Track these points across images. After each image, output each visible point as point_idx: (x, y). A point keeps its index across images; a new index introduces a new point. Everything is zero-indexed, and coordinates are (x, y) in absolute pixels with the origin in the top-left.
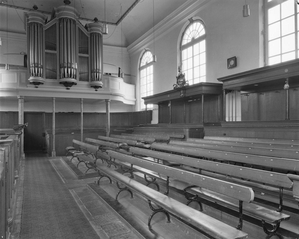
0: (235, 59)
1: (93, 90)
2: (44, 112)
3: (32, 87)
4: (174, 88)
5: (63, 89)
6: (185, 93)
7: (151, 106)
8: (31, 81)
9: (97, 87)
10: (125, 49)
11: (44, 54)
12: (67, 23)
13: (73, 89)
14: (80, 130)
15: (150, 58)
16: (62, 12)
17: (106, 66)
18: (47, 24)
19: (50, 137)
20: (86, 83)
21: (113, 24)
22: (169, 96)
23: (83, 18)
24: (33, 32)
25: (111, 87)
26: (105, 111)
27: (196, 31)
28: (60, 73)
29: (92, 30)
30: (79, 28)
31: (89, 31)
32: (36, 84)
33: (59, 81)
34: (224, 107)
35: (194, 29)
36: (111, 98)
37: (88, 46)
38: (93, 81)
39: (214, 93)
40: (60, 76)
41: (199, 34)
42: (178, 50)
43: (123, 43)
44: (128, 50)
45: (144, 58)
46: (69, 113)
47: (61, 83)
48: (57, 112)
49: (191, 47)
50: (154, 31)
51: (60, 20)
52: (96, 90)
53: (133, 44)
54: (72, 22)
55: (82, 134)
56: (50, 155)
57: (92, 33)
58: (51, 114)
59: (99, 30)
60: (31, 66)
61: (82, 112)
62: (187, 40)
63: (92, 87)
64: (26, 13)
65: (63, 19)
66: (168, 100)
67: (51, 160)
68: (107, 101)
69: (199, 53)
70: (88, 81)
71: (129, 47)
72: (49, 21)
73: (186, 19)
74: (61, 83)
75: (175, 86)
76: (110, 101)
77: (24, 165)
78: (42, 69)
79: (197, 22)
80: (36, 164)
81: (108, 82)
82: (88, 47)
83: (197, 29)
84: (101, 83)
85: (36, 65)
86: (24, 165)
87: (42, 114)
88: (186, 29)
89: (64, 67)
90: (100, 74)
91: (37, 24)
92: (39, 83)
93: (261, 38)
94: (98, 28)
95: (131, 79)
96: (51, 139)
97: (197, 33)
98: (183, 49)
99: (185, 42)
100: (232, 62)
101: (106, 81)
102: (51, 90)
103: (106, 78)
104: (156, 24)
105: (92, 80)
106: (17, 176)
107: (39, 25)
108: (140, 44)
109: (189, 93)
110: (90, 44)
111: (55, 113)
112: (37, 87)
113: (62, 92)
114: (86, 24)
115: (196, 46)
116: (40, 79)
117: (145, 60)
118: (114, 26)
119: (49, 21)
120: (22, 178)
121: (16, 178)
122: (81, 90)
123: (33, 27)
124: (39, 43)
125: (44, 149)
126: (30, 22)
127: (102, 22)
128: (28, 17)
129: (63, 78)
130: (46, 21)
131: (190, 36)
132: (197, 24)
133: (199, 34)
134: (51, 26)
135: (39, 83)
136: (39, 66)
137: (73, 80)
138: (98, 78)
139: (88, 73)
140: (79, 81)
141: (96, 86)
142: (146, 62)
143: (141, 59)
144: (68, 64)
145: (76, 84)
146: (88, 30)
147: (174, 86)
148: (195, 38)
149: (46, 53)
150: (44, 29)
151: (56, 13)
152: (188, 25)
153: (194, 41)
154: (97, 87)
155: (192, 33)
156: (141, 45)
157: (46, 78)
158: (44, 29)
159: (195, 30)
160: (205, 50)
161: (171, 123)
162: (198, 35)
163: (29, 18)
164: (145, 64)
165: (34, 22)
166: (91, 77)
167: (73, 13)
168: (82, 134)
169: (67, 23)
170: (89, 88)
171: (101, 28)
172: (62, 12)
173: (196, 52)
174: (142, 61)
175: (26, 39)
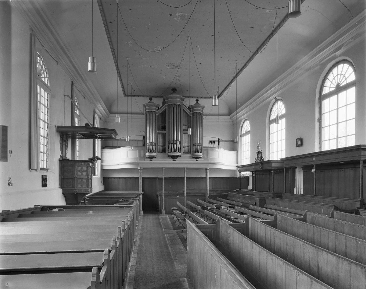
0: (301, 140)
1: (194, 161)
2: (158, 177)
3: (148, 161)
4: (256, 162)
5: (170, 161)
6: (262, 166)
7: (248, 173)
8: (147, 156)
9: (197, 158)
10: (229, 117)
11: (157, 133)
12: (174, 108)
13: (178, 160)
14: (183, 193)
15: (282, 109)
16: (170, 99)
17: (205, 137)
19: (161, 199)
20: (189, 155)
22: (314, 159)
24: (149, 120)
25: (210, 157)
26: (205, 176)
27: (342, 76)
28: (168, 148)
29: (193, 110)
32: (151, 158)
33: (167, 154)
34: (90, 183)
35: (340, 73)
36: (209, 167)
37: (191, 123)
38: (194, 153)
39: (287, 167)
40: (168, 150)
41: (346, 79)
42: (267, 124)
44: (231, 118)
45: (274, 109)
46: (170, 178)
47: (169, 156)
48: (168, 176)
49: (336, 96)
50: (277, 83)
51: (169, 105)
52: (197, 161)
53: (235, 113)
54: (178, 106)
55: (185, 197)
56: (161, 213)
58: (162, 178)
59: (200, 110)
60: (147, 144)
61: (208, 176)
62: (329, 86)
63: (193, 158)
65: (171, 105)
66: (271, 169)
67: (160, 217)
68: (206, 169)
69: (345, 105)
70: (190, 153)
71: (231, 115)
72: (161, 108)
74: (169, 156)
75: (256, 160)
76: (209, 169)
77: (142, 219)
78: (155, 146)
79: (344, 63)
80: (151, 218)
81: (208, 153)
83: (343, 73)
84: (201, 154)
85: (151, 144)
86: (142, 219)
87: (156, 179)
89: (172, 144)
90: (200, 147)
91: (152, 112)
92: (153, 157)
93: (317, 124)
95: (233, 146)
96: (163, 202)
97: (344, 79)
98: (271, 124)
99: (326, 91)
100: (299, 143)
101: (205, 152)
102: (162, 162)
103: (206, 150)
104: (238, 109)
105: (194, 152)
106: (137, 224)
108: (242, 114)
109: (266, 167)
110: (193, 118)
111: (165, 178)
112: (151, 160)
113: (168, 163)
114: (189, 106)
115: (342, 95)
116: (154, 154)
117: (276, 112)
119: (161, 108)
120: (140, 227)
121: (137, 226)
122: (185, 161)
123: (149, 115)
124: (153, 127)
125: (158, 208)
126: (147, 111)
128: (146, 107)
129: (170, 152)
130: (158, 108)
131: (334, 82)
132: (343, 66)
133: (346, 79)
134: (162, 112)
135: (153, 157)
136: (153, 144)
137: (178, 154)
138: (198, 150)
139: (191, 146)
140: (183, 153)
141: (196, 157)
142: (277, 114)
143: (242, 127)
144: (174, 141)
145: (180, 156)
147: (255, 159)
148: (341, 86)
149: (158, 133)
150: (157, 115)
151: (166, 101)
153: (339, 89)
154: (197, 158)
155: (336, 78)
156: (267, 96)
157: (158, 153)
158: (157, 115)
159: (341, 74)
160: (354, 101)
161: (316, 195)
162: (345, 80)
164: (245, 132)
166: (193, 149)
168: (185, 197)
169: (174, 108)
170: (191, 159)
172: (170, 99)
173: (342, 103)
174: (272, 113)
175: (144, 119)
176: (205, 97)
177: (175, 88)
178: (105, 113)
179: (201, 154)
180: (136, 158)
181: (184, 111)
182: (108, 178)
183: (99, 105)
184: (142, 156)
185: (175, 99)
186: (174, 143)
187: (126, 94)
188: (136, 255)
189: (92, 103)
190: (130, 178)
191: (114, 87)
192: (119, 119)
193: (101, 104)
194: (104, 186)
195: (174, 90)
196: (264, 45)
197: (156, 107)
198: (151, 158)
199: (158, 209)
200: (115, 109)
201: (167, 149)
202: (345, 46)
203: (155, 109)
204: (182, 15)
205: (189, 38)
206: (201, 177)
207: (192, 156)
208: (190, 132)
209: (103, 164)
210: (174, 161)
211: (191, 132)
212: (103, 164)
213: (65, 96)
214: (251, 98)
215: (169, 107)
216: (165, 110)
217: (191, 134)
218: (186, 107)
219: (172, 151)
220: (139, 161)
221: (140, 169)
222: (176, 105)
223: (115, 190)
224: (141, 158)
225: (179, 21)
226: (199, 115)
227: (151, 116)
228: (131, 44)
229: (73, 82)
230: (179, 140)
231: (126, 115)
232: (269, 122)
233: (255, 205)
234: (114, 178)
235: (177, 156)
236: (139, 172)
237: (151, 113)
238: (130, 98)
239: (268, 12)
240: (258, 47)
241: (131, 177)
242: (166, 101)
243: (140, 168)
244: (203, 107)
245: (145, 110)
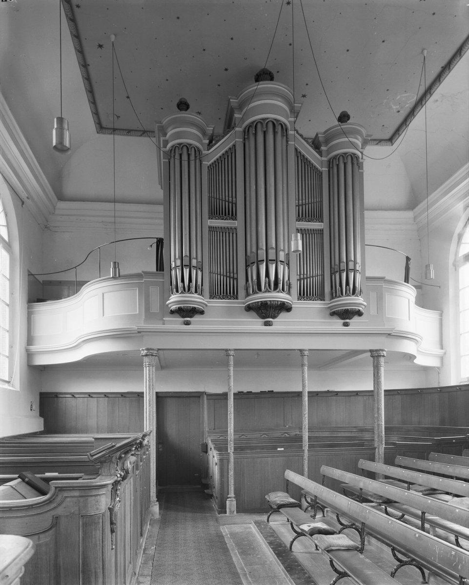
1: (337, 324)
3: (176, 324)
5: (255, 324)
8: (173, 307)
10: (410, 214)
13: (281, 322)
14: (299, 439)
17: (377, 246)
20: (317, 305)
28: (247, 280)
30: (296, 149)
31: (323, 153)
32: (187, 312)
40: (247, 289)
44: (415, 218)
47: (249, 308)
59: (354, 146)
60: (173, 266)
63: (333, 314)
68: (375, 355)
70: (322, 298)
74: (249, 308)
78: (200, 273)
81: (380, 299)
84: (359, 300)
90: (358, 276)
91: (188, 147)
102: (227, 327)
112: (187, 323)
116: (195, 300)
134: (226, 152)
140: (298, 299)
141: (347, 311)
150: (206, 163)
154: (346, 314)
158: (206, 163)
163: (169, 134)
169: (265, 133)
175: (162, 221)
178: (44, 197)
179: (359, 300)
180: (132, 317)
182: (56, 395)
184: (155, 308)
185: (268, 104)
186: (270, 258)
187: (104, 124)
188: (152, 500)
190: (123, 395)
194: (42, 420)
198: (187, 312)
199: (207, 488)
201: (238, 280)
206: (332, 392)
207: (329, 308)
209: (33, 348)
210: (267, 324)
212: (33, 348)
215: (248, 138)
216: (233, 149)
219: (260, 289)
220: (143, 325)
221: (146, 355)
223: (76, 431)
224: (149, 315)
227: (185, 164)
230: (283, 250)
233: (372, 459)
234: (73, 395)
235: (284, 308)
236: (146, 371)
241: (126, 391)
242: (236, 115)
243: (148, 349)
245: (165, 147)
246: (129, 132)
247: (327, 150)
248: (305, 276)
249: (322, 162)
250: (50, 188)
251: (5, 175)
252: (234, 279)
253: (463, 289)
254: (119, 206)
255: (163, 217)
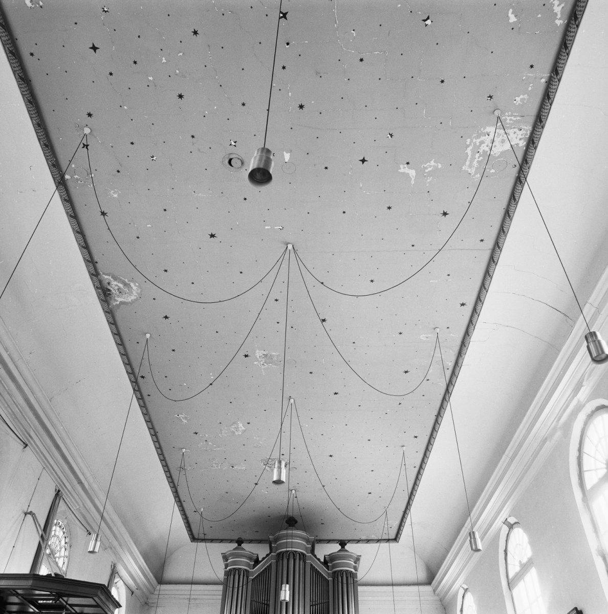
10: (428, 589)
18: (256, 568)
21: (388, 540)
23: (330, 539)
24: (231, 589)
29: (334, 566)
30: (311, 565)
31: (330, 568)
37: (328, 599)
43: (422, 575)
44: (434, 591)
57: (335, 572)
59: (348, 565)
64: (224, 554)
71: (435, 582)
73: (498, 524)
82: (328, 602)
88: (506, 541)
94: (348, 561)
107: (242, 572)
118: (393, 545)
127: (366, 540)
128: (227, 560)
146: (328, 567)
152: (508, 533)
158: (251, 578)
163: (229, 561)
165: (234, 569)
167: (304, 543)
171: (352, 560)
176: (365, 540)
177: (293, 517)
181: (312, 567)
183: (128, 554)
185: (296, 542)
189: (109, 549)
191: (166, 520)
192: (98, 543)
193: (131, 554)
195: (291, 522)
196: (444, 407)
197: (250, 558)
200: (172, 573)
202: (587, 379)
203: (248, 565)
204: (266, 356)
205: (292, 401)
208: (285, 593)
211: (288, 592)
213: (26, 514)
214: (460, 532)
216: (270, 567)
217: (287, 599)
218: (319, 560)
222: (294, 554)
225: (263, 367)
226: (347, 578)
228: (186, 418)
229: (59, 491)
231: (188, 587)
232: (509, 584)
237: (237, 572)
238: (202, 545)
239: (425, 339)
240: (436, 413)
244: (357, 560)
246: (212, 541)
247: (332, 566)
248: (314, 603)
249: (328, 573)
250: (154, 579)
251: (127, 584)
252: (267, 604)
253: (486, 250)
254: (194, 587)
255: (222, 589)
